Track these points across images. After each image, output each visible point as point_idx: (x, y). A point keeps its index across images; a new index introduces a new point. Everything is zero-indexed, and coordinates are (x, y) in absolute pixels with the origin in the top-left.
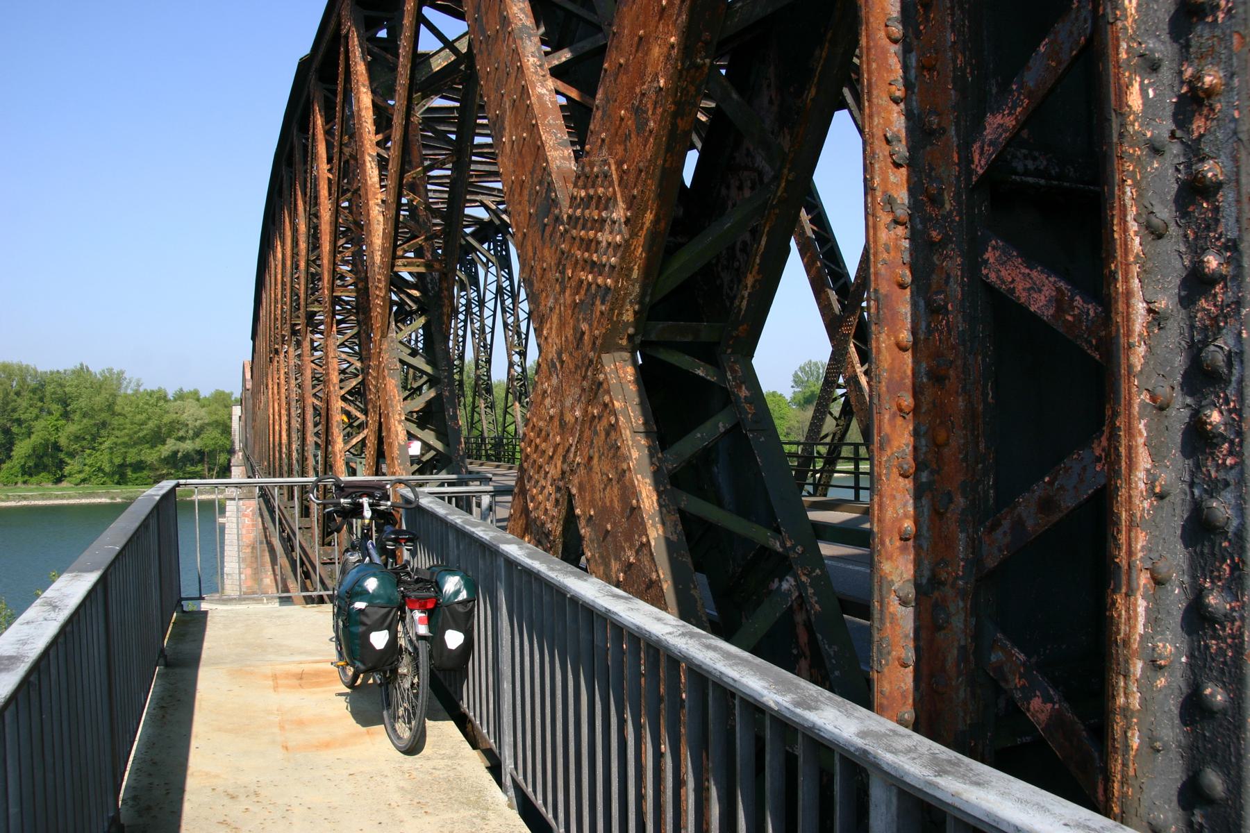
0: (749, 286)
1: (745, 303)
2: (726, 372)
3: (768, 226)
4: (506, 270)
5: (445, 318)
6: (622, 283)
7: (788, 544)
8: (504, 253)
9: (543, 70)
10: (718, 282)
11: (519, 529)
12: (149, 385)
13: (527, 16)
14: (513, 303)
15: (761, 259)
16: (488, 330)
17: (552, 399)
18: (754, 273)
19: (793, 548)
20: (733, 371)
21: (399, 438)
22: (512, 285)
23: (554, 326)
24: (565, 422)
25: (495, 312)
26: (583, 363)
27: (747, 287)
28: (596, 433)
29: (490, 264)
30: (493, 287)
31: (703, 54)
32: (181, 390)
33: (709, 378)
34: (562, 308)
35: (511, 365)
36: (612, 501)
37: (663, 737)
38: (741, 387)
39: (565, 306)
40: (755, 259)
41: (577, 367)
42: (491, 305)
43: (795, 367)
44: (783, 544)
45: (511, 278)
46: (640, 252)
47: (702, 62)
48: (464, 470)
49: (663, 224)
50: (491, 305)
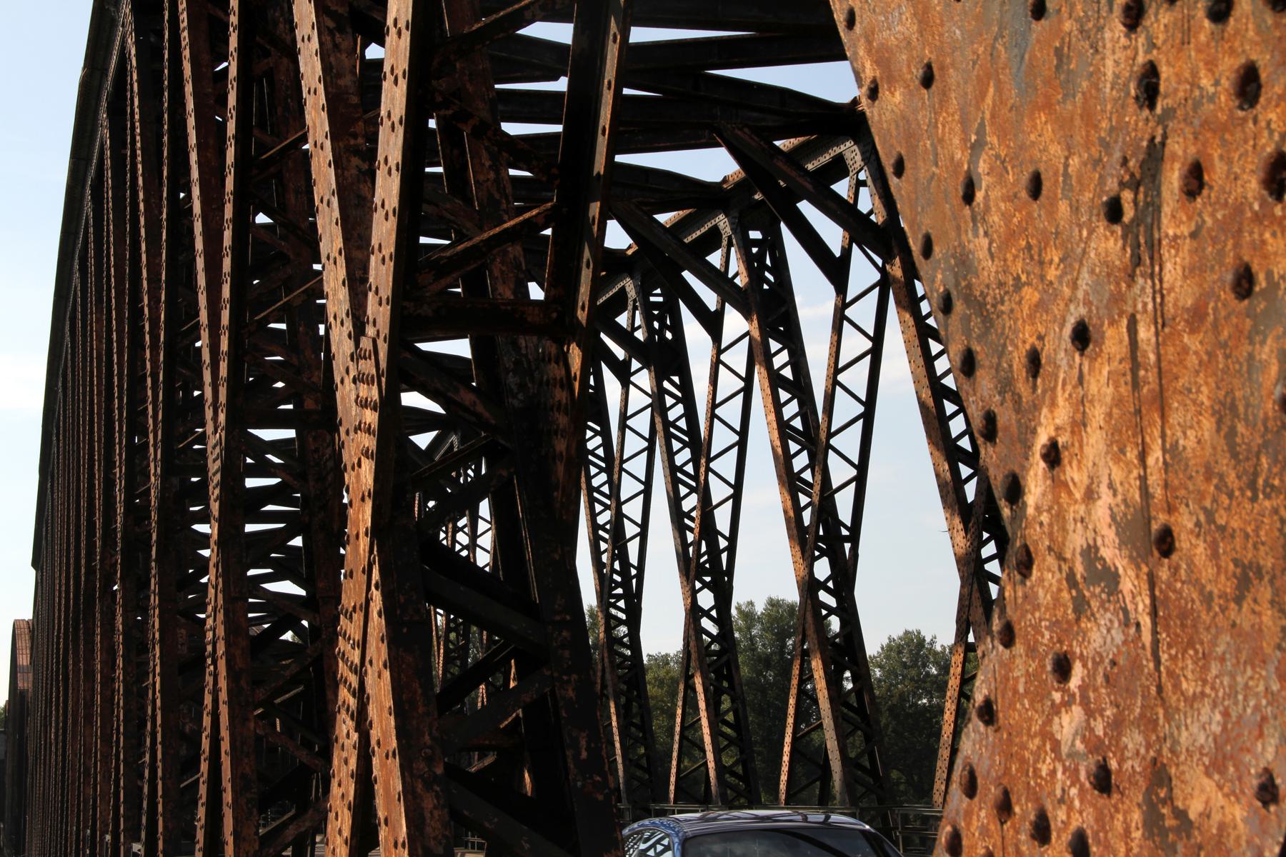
4: (676, 379)
5: (560, 468)
8: (669, 335)
14: (695, 460)
16: (631, 530)
17: (1090, 714)
21: (428, 830)
22: (691, 414)
23: (1097, 415)
24: (1181, 815)
25: (648, 483)
29: (635, 365)
30: (642, 423)
34: (1145, 333)
35: (694, 612)
37: (350, 627)
39: (1161, 320)
42: (637, 466)
43: (912, 627)
50: (637, 466)
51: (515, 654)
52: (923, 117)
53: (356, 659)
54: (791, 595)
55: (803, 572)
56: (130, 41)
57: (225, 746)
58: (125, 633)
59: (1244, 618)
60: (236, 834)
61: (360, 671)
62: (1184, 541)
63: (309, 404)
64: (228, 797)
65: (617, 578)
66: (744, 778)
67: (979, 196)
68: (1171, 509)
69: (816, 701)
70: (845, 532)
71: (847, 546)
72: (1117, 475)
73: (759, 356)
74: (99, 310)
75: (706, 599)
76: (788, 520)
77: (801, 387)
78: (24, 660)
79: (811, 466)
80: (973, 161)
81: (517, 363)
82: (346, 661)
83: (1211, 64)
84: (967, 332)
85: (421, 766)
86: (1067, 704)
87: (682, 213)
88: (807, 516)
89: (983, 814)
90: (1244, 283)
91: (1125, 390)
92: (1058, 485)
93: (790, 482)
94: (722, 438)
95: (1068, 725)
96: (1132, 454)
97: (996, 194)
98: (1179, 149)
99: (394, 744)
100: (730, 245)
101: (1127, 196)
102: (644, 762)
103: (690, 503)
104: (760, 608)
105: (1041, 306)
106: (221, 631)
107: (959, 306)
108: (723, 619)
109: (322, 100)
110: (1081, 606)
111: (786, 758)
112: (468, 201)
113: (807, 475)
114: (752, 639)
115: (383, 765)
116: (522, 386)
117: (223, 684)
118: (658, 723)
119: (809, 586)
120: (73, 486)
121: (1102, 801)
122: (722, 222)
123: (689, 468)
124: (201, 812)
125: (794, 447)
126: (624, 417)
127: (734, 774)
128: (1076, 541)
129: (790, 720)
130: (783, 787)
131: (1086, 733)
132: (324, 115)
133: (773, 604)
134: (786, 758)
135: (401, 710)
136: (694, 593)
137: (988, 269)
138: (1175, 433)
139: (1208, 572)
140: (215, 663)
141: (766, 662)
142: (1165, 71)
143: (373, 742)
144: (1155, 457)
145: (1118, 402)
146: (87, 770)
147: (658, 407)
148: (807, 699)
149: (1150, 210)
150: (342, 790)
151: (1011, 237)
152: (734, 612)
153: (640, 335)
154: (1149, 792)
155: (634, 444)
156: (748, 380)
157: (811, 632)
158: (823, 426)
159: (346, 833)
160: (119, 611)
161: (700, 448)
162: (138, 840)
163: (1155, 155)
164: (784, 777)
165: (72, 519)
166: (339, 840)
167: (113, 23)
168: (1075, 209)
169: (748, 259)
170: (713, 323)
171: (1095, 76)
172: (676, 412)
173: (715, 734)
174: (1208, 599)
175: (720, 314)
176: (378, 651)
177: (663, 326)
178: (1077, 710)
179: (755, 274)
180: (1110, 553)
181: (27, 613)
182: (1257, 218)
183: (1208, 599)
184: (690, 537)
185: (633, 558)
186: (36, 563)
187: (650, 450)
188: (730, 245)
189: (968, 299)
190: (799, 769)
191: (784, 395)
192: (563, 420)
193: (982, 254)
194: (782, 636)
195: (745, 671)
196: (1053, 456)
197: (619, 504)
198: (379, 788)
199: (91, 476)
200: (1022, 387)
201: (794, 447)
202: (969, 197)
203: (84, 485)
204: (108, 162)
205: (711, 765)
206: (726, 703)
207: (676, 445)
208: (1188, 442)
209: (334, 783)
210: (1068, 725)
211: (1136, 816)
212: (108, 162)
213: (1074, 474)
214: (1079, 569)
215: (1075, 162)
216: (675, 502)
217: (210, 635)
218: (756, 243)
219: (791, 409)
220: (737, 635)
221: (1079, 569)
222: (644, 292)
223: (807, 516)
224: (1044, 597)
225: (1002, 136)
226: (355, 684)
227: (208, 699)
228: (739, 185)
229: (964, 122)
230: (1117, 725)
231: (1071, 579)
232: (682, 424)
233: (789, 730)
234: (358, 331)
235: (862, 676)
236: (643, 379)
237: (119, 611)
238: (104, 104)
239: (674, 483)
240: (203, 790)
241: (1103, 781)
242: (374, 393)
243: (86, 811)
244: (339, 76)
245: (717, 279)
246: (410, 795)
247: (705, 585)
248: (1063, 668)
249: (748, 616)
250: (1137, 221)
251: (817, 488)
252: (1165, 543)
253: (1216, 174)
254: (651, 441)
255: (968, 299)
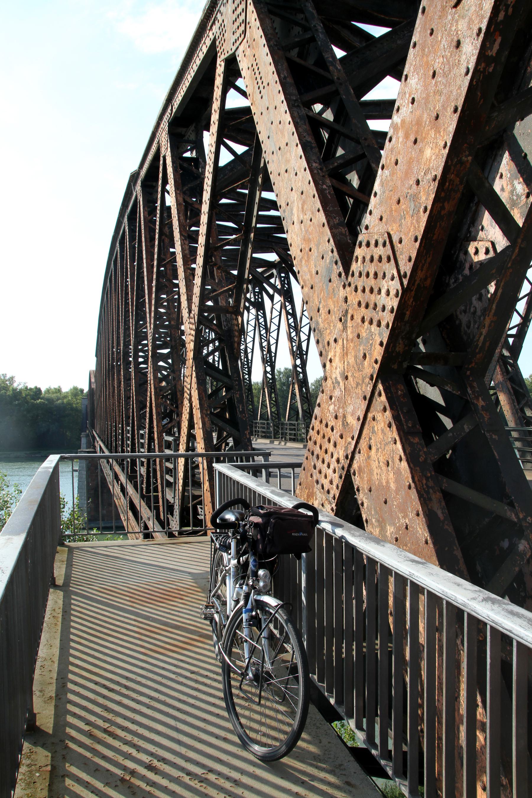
0: (486, 326)
1: (482, 337)
2: (467, 388)
3: (503, 281)
4: (262, 311)
5: (236, 345)
6: (397, 324)
7: (521, 516)
8: (260, 300)
9: (323, 172)
10: (457, 322)
11: (305, 496)
12: (33, 387)
13: (308, 134)
14: (266, 333)
15: (497, 306)
16: (249, 350)
17: (335, 406)
18: (490, 316)
19: (525, 519)
20: (472, 387)
23: (337, 354)
24: (347, 423)
25: (254, 339)
26: (363, 381)
27: (484, 326)
28: (374, 432)
29: (251, 307)
30: (252, 323)
31: (467, 153)
32: (12, 379)
33: (454, 392)
34: (345, 342)
35: (265, 372)
36: (388, 482)
38: (478, 400)
39: (347, 340)
40: (492, 306)
41: (358, 384)
42: (251, 334)
44: (517, 515)
45: (265, 317)
46: (411, 301)
47: (466, 159)
48: (250, 448)
49: (428, 282)
51: (225, 387)
52: (311, 294)
53: (189, 387)
54: (290, 367)
55: (293, 363)
56: (127, 228)
57: (154, 405)
58: (124, 376)
59: (357, 392)
60: (157, 425)
61: (190, 390)
62: (349, 378)
63: (172, 323)
64: (155, 417)
65: (246, 363)
66: (277, 414)
67: (320, 311)
68: (348, 372)
69: (296, 395)
70: (304, 353)
71: (305, 356)
72: (340, 365)
73: (283, 307)
74: (115, 293)
75: (269, 369)
76: (290, 349)
77: (294, 315)
78: (93, 380)
79: (296, 335)
80: (319, 304)
81: (226, 319)
82: (186, 387)
83: (355, 299)
84: (318, 336)
85: (205, 412)
86: (331, 404)
87: (264, 269)
88: (295, 349)
89: (318, 423)
90: (358, 336)
91: (342, 351)
92: (331, 366)
93: (291, 339)
94: (273, 327)
95: (332, 408)
96: (342, 362)
97: (323, 312)
98: (350, 312)
99: (199, 406)
100: (276, 277)
101: (343, 318)
102: (252, 410)
103: (265, 344)
104: (282, 370)
105: (330, 333)
106: (152, 378)
107: (316, 331)
108: (273, 374)
109: (181, 256)
110: (334, 387)
111: (288, 410)
112: (214, 279)
113: (295, 338)
114: (280, 378)
115: (196, 411)
116: (227, 325)
117: (153, 390)
118: (255, 399)
119: (295, 366)
120: (107, 337)
121: (336, 420)
122: (274, 271)
123: (265, 335)
124: (147, 420)
125: (292, 330)
126: (248, 321)
127: (274, 413)
128: (334, 376)
129: (289, 400)
130: (287, 417)
131: (334, 409)
132: (182, 260)
133: (286, 369)
134: (288, 410)
135: (200, 399)
136: (265, 367)
137: (321, 325)
138: (349, 360)
139: (352, 383)
140: (150, 385)
141: (284, 384)
142: (348, 298)
143: (193, 406)
144: (346, 363)
145: (341, 353)
146: (113, 410)
147: (257, 319)
148: (294, 395)
149: (346, 321)
150: (185, 416)
151: (325, 320)
152: (276, 371)
153: (253, 300)
154: (343, 419)
155: (250, 328)
156: (280, 312)
157: (295, 378)
158: (299, 325)
159: (187, 426)
160: (122, 370)
161: (267, 330)
162: (129, 426)
163: (347, 311)
164: (287, 414)
165: (107, 346)
166: (185, 427)
167: (122, 223)
168: (335, 318)
169: (281, 281)
170: (271, 298)
171: (339, 295)
172: (262, 320)
173: (270, 403)
174: (352, 388)
175: (273, 296)
176: (194, 386)
177: (258, 297)
178: (333, 405)
179: (283, 285)
180: (339, 379)
181: (94, 368)
182: (361, 326)
183: (352, 388)
184: (265, 353)
185: (250, 358)
186: (96, 356)
187: (255, 330)
188: (276, 277)
189: (318, 330)
190: (292, 412)
191: (289, 317)
192: (237, 334)
193: (320, 322)
194: (288, 378)
195: (278, 386)
196: (331, 361)
197: (246, 344)
198: (195, 417)
199: (113, 335)
200: (326, 347)
201: (292, 330)
202: (318, 311)
203: (111, 337)
204: (119, 256)
205: (269, 411)
206: (273, 395)
207: (261, 329)
208: (350, 361)
209: (183, 415)
210: (332, 408)
211: (341, 423)
212: (119, 256)
213: (334, 364)
214: (334, 381)
215: (335, 309)
216: (261, 344)
217: (149, 379)
218: (283, 277)
219: (291, 320)
220: (276, 377)
221: (334, 381)
222: (254, 289)
223: (295, 349)
224: (329, 385)
225: (324, 302)
226: (189, 393)
227: (149, 394)
228: (279, 262)
229: (318, 297)
230: (339, 408)
231: (333, 382)
232: (263, 323)
233: (289, 403)
234: (190, 311)
235: (307, 389)
236: (253, 311)
237: (122, 370)
238: (118, 242)
239: (261, 338)
240: (148, 415)
241: (336, 417)
242: (194, 327)
243: (113, 419)
244: (185, 250)
245: (273, 286)
246: (202, 418)
247: (268, 365)
248: (331, 398)
249: (279, 372)
250: (344, 322)
251: (297, 341)
252: (347, 378)
253: (355, 317)
254: (255, 327)
255: (318, 330)
